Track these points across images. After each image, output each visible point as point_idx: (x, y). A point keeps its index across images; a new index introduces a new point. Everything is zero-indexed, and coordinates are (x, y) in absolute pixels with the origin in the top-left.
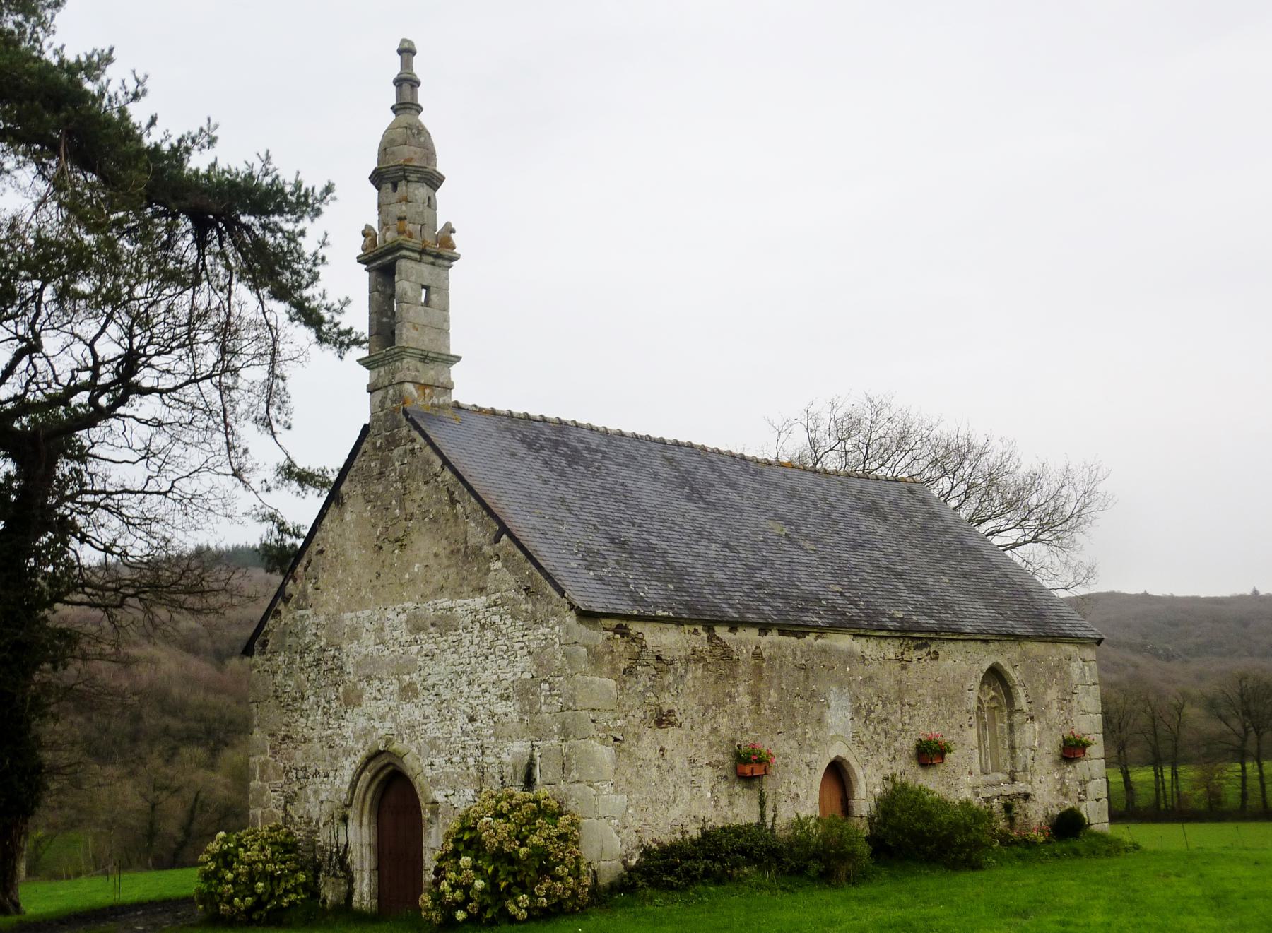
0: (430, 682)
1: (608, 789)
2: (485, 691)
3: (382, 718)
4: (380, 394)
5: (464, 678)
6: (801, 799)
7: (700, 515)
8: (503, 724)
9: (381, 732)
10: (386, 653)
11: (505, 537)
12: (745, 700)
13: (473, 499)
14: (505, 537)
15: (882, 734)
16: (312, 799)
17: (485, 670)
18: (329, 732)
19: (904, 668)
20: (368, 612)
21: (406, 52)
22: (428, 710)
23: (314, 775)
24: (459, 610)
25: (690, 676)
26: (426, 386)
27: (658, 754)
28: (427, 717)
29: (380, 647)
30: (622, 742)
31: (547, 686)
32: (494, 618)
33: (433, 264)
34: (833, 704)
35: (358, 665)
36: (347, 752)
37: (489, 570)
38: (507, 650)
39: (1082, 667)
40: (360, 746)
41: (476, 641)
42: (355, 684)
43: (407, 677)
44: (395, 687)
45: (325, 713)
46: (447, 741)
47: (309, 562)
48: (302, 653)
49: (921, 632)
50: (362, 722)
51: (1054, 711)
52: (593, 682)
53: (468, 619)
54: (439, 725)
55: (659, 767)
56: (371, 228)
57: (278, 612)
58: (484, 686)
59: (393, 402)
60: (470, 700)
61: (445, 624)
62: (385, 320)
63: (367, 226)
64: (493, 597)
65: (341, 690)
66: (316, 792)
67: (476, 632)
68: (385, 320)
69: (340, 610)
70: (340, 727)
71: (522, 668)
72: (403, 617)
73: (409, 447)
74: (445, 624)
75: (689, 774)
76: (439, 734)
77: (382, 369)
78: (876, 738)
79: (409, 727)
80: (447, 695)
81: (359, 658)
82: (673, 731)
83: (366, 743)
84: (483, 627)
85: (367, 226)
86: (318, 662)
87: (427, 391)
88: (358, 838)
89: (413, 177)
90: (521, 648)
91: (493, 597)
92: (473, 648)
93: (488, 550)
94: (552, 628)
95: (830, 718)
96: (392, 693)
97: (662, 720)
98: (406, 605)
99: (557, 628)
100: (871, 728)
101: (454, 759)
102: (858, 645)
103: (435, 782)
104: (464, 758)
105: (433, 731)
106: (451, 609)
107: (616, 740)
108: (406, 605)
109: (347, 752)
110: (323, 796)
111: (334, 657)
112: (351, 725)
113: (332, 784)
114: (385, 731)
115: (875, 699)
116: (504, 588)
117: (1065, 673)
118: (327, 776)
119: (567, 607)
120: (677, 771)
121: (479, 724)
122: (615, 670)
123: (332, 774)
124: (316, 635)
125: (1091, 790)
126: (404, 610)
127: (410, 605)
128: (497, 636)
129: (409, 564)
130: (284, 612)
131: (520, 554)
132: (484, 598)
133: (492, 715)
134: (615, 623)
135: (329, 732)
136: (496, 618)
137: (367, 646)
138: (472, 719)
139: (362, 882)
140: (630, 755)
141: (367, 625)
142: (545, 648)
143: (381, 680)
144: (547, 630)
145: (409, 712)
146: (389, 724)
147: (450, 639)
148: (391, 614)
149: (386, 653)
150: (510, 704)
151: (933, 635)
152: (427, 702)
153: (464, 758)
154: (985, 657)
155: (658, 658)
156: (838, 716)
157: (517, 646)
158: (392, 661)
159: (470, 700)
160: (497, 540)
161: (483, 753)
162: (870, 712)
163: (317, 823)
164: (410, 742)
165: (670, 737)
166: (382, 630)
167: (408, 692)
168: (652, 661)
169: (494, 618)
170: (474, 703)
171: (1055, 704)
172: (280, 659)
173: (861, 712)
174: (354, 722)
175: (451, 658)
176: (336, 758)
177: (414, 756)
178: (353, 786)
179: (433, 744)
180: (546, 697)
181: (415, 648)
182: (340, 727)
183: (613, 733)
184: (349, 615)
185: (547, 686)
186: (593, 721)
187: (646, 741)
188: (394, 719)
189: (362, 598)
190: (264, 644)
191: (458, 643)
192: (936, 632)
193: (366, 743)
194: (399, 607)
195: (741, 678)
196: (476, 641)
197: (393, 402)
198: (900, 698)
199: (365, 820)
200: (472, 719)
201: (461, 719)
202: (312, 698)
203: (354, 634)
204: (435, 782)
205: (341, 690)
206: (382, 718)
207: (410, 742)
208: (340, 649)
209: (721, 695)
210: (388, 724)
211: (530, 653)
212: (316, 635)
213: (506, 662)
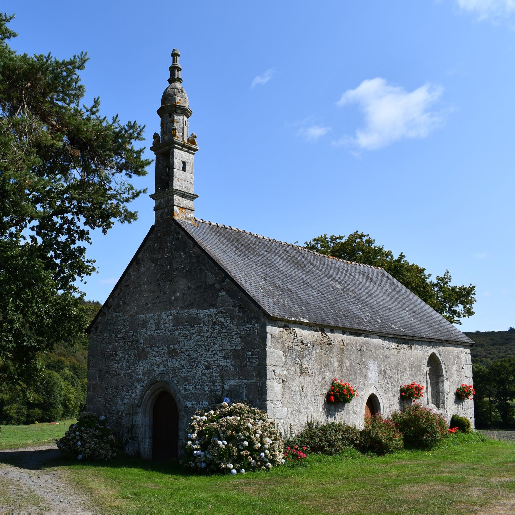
0: (185, 349)
1: (279, 404)
2: (214, 354)
3: (159, 365)
4: (160, 211)
5: (204, 347)
6: (358, 413)
7: (304, 276)
8: (225, 371)
9: (157, 372)
10: (161, 334)
11: (227, 280)
12: (336, 364)
13: (210, 262)
14: (227, 280)
15: (390, 384)
16: (120, 402)
17: (215, 344)
18: (129, 371)
19: (398, 353)
20: (152, 315)
21: (174, 55)
22: (183, 363)
23: (121, 391)
24: (201, 315)
25: (314, 352)
26: (183, 208)
27: (301, 389)
28: (183, 366)
29: (158, 331)
30: (286, 382)
31: (250, 353)
32: (220, 319)
33: (186, 151)
34: (371, 369)
35: (146, 340)
36: (139, 381)
37: (218, 296)
38: (228, 335)
39: (465, 355)
40: (146, 378)
41: (211, 330)
42: (144, 349)
43: (172, 346)
44: (166, 350)
45: (128, 362)
46: (193, 377)
47: (121, 290)
48: (116, 333)
49: (406, 336)
50: (148, 367)
51: (455, 376)
52: (274, 352)
53: (206, 319)
54: (189, 370)
55: (301, 395)
56: (158, 134)
57: (105, 314)
58: (214, 352)
59: (167, 215)
60: (207, 358)
61: (193, 321)
62: (163, 177)
63: (155, 133)
64: (221, 309)
65: (136, 351)
66: (122, 399)
67: (211, 326)
68: (163, 177)
69: (137, 313)
70: (135, 369)
71: (236, 343)
72: (171, 317)
73: (176, 236)
74: (193, 321)
75: (313, 399)
76: (189, 374)
77: (162, 200)
78: (388, 385)
79: (172, 370)
80: (194, 356)
81: (146, 336)
82: (308, 379)
83: (149, 377)
84: (214, 323)
85: (155, 133)
86: (124, 338)
87: (183, 211)
88: (142, 421)
89: (179, 111)
90: (236, 334)
91: (221, 309)
92: (208, 334)
93: (217, 286)
94: (254, 325)
95: (370, 375)
96: (164, 354)
97: (303, 371)
98: (172, 312)
99: (256, 325)
100: (386, 380)
101: (197, 387)
102: (380, 341)
103: (186, 398)
104: (203, 386)
105: (185, 372)
106: (197, 314)
107: (283, 381)
108: (172, 312)
109: (139, 381)
110: (126, 401)
111: (133, 335)
112: (142, 368)
113: (131, 396)
114: (160, 372)
115: (387, 367)
116: (226, 305)
117: (459, 358)
118: (128, 392)
119: (262, 314)
120: (309, 397)
121: (211, 370)
122: (283, 347)
123: (130, 391)
124: (123, 325)
125: (467, 411)
126: (171, 314)
127: (174, 311)
128: (222, 328)
129: (175, 292)
130: (107, 313)
131: (236, 288)
132: (215, 309)
133: (219, 366)
134: (284, 324)
135: (129, 371)
136: (222, 319)
137: (152, 331)
138: (207, 368)
139: (145, 443)
140: (289, 388)
141: (151, 321)
142: (249, 335)
143: (158, 347)
144: (250, 326)
145: (173, 363)
146: (161, 369)
147: (196, 329)
148: (164, 316)
149: (161, 334)
150: (229, 361)
151: (411, 338)
152: (183, 358)
153: (203, 386)
154: (430, 350)
155: (302, 342)
156: (373, 372)
157: (233, 333)
158: (164, 338)
159: (207, 358)
160: (223, 281)
161: (213, 385)
162: (385, 373)
163: (122, 414)
164: (173, 377)
165: (306, 380)
166: (159, 323)
167: (172, 354)
168: (300, 344)
169: (220, 319)
170: (209, 360)
171: (456, 373)
172: (105, 335)
173: (382, 373)
174: (143, 366)
175: (196, 337)
176: (133, 383)
177: (175, 384)
178: (142, 397)
179: (185, 379)
180: (249, 358)
181: (177, 333)
182: (135, 369)
183: (282, 377)
184: (142, 316)
185: (250, 353)
186: (274, 371)
187: (296, 383)
188: (164, 366)
189: (149, 308)
190: (97, 328)
191: (200, 332)
192: (412, 336)
193: (149, 377)
194: (168, 313)
195: (335, 354)
196: (211, 330)
197: (167, 215)
198: (397, 367)
199: (147, 414)
200: (207, 368)
201: (201, 368)
202: (121, 355)
203: (144, 324)
204: (186, 398)
205: (136, 351)
206: (159, 365)
207: (173, 377)
208: (137, 332)
209: (327, 362)
210: (161, 369)
211: (240, 337)
212: (123, 325)
213: (227, 341)
